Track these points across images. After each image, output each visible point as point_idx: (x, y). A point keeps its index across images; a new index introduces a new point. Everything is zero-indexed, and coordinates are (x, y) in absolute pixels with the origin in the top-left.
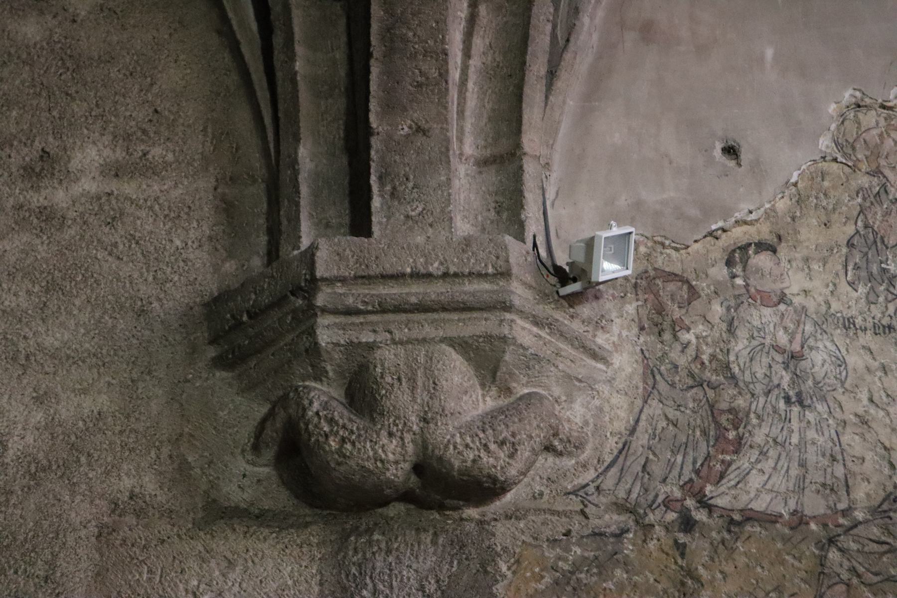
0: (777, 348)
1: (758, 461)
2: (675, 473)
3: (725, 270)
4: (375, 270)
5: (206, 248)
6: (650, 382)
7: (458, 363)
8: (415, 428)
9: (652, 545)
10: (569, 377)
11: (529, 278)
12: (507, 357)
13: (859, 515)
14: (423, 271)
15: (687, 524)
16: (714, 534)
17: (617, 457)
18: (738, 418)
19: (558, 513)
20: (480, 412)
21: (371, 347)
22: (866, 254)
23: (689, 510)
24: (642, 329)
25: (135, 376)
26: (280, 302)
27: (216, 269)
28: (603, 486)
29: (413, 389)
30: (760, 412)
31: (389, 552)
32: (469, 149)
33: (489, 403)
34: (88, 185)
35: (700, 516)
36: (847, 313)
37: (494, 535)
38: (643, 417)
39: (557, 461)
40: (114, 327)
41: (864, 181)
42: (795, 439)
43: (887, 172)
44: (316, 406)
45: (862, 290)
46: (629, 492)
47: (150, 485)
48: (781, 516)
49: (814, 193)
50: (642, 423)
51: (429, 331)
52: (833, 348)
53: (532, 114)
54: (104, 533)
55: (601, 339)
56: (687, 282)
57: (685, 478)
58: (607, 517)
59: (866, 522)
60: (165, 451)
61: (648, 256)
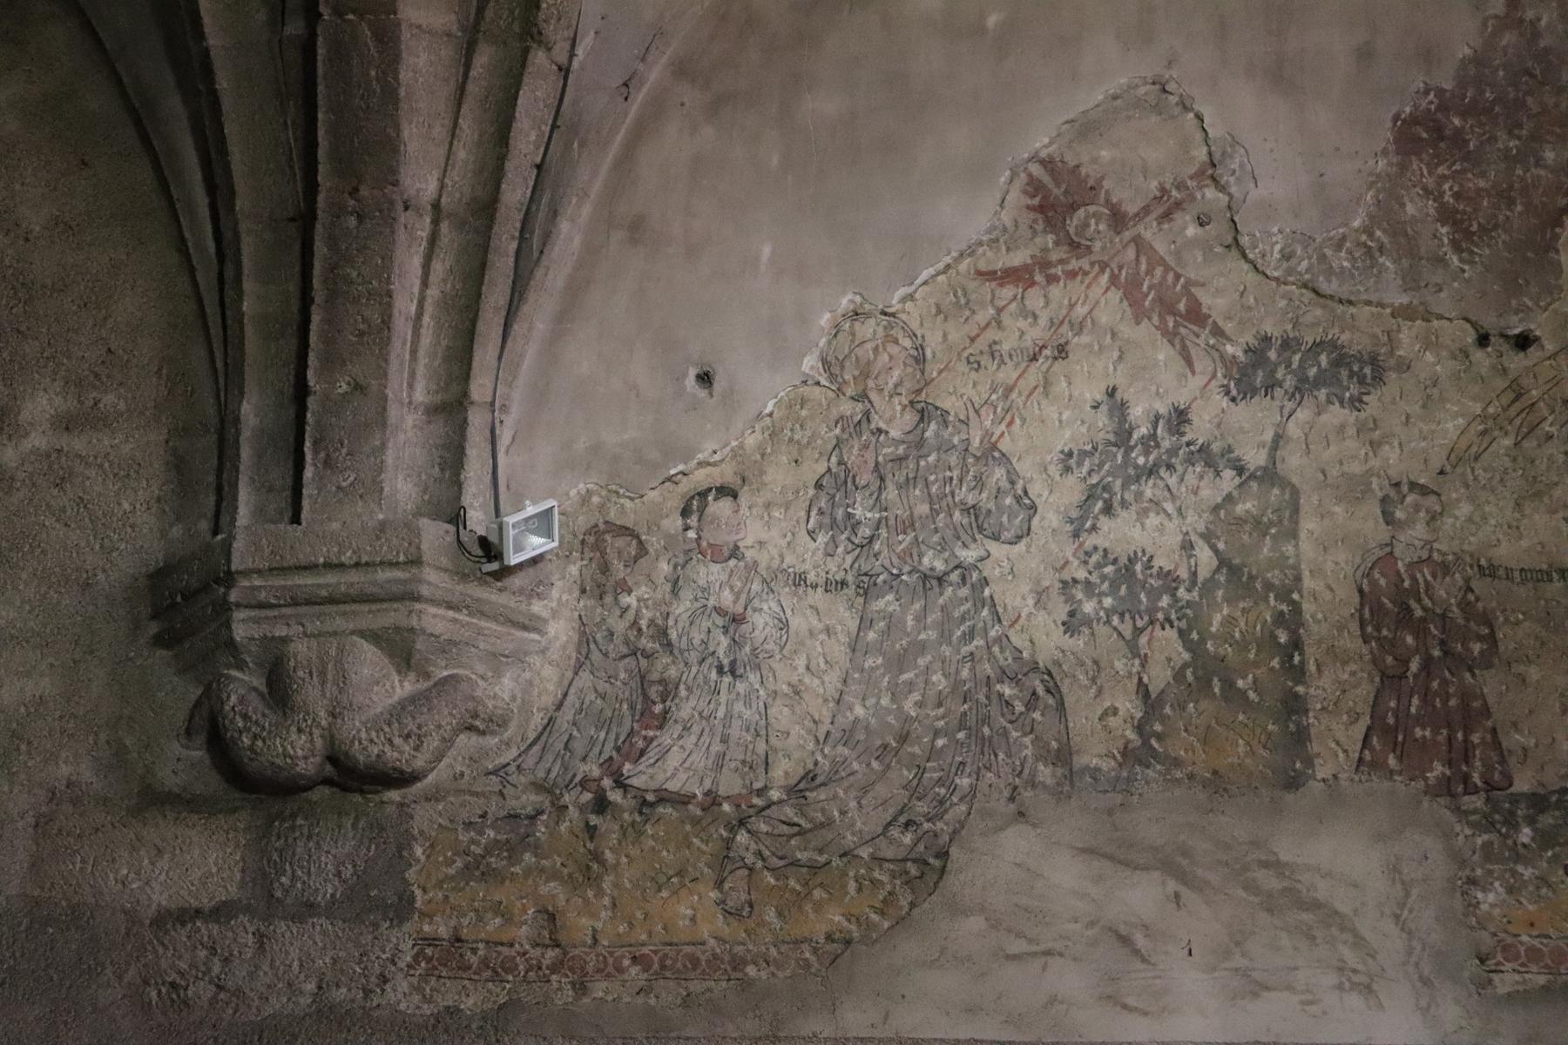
0: (719, 610)
1: (680, 737)
2: (596, 750)
3: (680, 522)
4: (290, 561)
5: (154, 510)
6: (584, 652)
7: (369, 655)
8: (324, 723)
9: (564, 827)
10: (494, 655)
11: (444, 561)
12: (418, 646)
13: (775, 795)
14: (335, 561)
15: (601, 805)
16: (626, 816)
17: (541, 734)
18: (669, 690)
19: (477, 794)
20: (396, 698)
21: (285, 640)
22: (833, 497)
23: (604, 791)
24: (583, 591)
25: (77, 657)
26: (205, 588)
27: (163, 534)
28: (524, 766)
29: (323, 683)
30: (690, 682)
31: (309, 837)
32: (420, 395)
33: (404, 687)
34: (37, 441)
35: (615, 796)
36: (800, 568)
37: (412, 817)
38: (572, 691)
39: (481, 740)
40: (59, 603)
41: (846, 407)
42: (720, 714)
43: (873, 396)
44: (233, 698)
45: (822, 539)
46: (549, 771)
47: (87, 774)
48: (695, 796)
49: (789, 425)
50: (571, 698)
51: (340, 623)
52: (778, 610)
53: (485, 354)
54: (42, 824)
55: (537, 607)
56: (638, 537)
57: (605, 756)
58: (524, 797)
59: (780, 802)
60: (103, 737)
61: (602, 507)
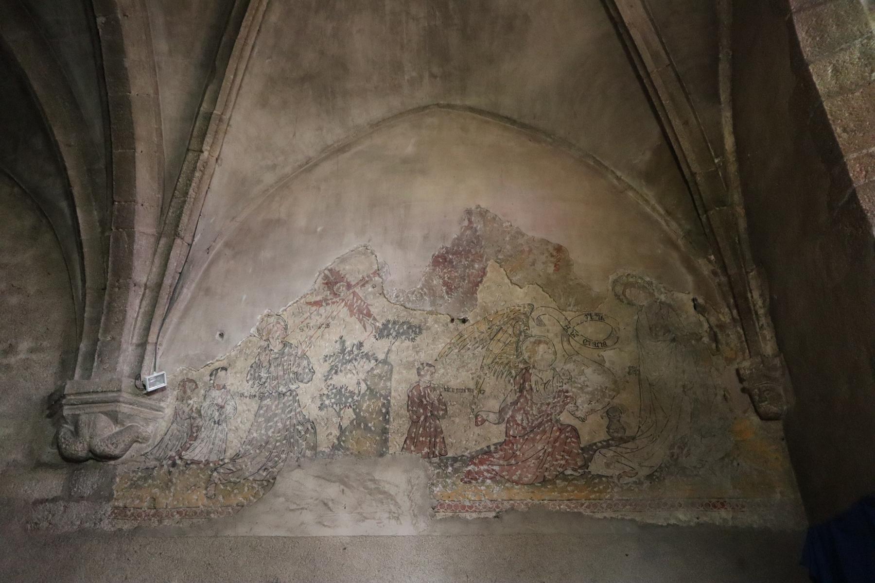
4: (82, 391)
15: (174, 464)
18: (199, 429)
21: (79, 415)
34: (22, 356)
35: (179, 462)
45: (251, 382)
51: (96, 410)
